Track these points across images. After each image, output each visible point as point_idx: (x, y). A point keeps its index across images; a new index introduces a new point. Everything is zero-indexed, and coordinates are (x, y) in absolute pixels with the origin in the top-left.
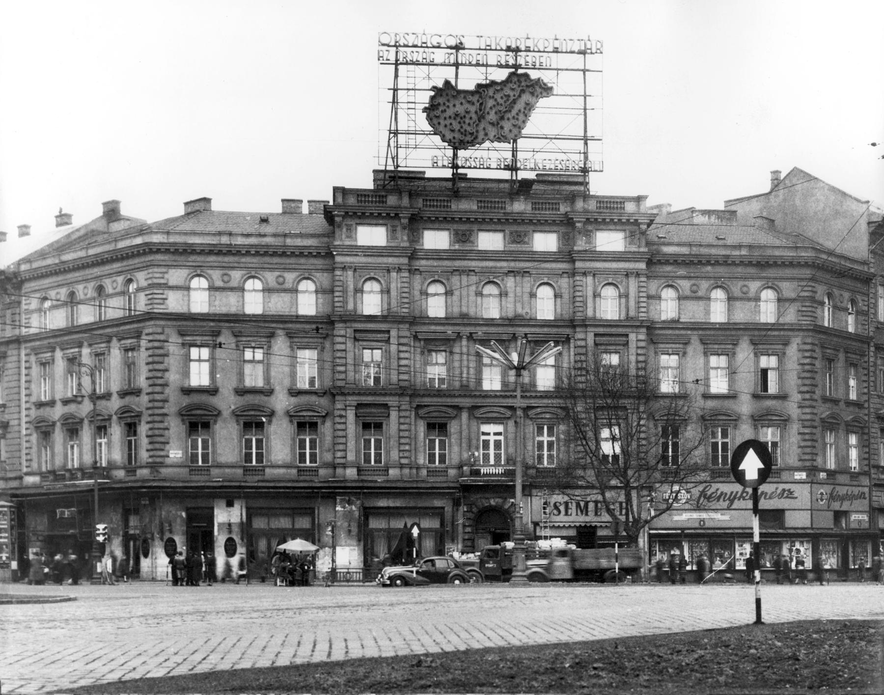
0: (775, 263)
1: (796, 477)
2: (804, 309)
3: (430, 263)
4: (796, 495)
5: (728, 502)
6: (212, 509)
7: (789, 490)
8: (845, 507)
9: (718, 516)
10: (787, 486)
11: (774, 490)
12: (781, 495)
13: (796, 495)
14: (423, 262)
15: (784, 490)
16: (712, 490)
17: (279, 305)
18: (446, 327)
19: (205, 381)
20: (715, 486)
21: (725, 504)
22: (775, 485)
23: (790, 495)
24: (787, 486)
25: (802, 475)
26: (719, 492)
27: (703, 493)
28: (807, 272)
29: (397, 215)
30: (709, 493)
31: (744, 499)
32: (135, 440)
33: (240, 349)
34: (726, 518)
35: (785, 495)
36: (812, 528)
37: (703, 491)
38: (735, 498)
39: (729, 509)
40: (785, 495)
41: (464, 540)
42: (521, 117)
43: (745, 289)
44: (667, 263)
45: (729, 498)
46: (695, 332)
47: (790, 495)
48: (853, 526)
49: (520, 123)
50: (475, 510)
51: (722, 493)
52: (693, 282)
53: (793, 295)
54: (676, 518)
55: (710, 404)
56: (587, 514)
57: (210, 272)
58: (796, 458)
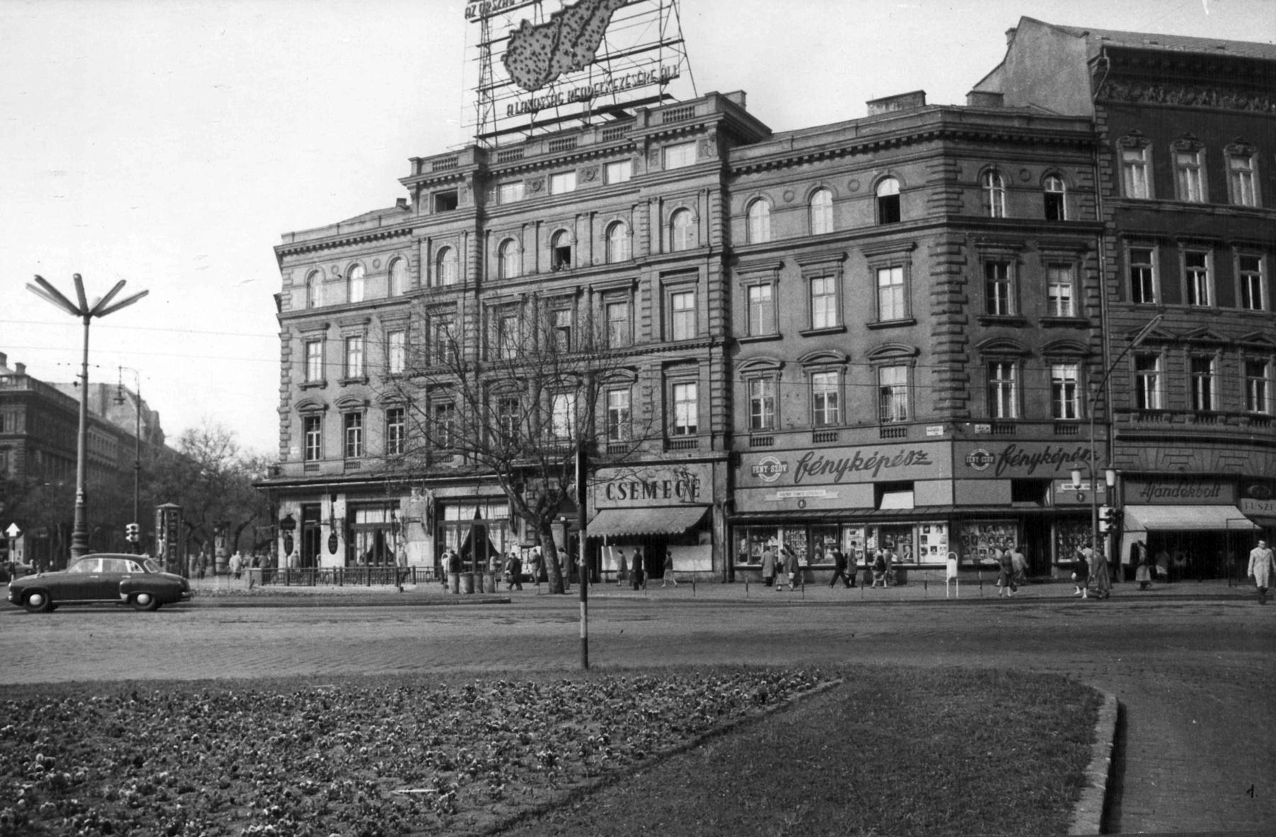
0: (888, 142)
1: (929, 434)
2: (935, 197)
3: (503, 220)
4: (929, 459)
5: (835, 474)
6: (319, 505)
7: (920, 453)
8: (1041, 472)
9: (822, 493)
10: (916, 448)
11: (898, 453)
12: (909, 461)
13: (929, 459)
14: (495, 221)
15: (913, 453)
16: (815, 458)
17: (792, 226)
18: (513, 289)
19: (832, 323)
20: (818, 454)
21: (830, 477)
22: (900, 447)
23: (922, 459)
24: (916, 448)
25: (939, 431)
26: (824, 462)
27: (802, 463)
28: (937, 145)
29: (702, 125)
30: (811, 463)
31: (857, 469)
32: (318, 436)
33: (876, 270)
34: (834, 495)
35: (915, 459)
36: (955, 506)
37: (803, 461)
38: (845, 468)
39: (836, 483)
40: (915, 459)
41: (527, 532)
42: (596, 37)
43: (854, 185)
44: (749, 171)
45: (837, 470)
46: (790, 252)
47: (922, 459)
48: (1060, 501)
49: (594, 45)
50: (537, 496)
51: (828, 463)
52: (374, 258)
53: (921, 182)
54: (769, 497)
55: (813, 342)
56: (655, 497)
57: (899, 169)
58: (931, 406)
